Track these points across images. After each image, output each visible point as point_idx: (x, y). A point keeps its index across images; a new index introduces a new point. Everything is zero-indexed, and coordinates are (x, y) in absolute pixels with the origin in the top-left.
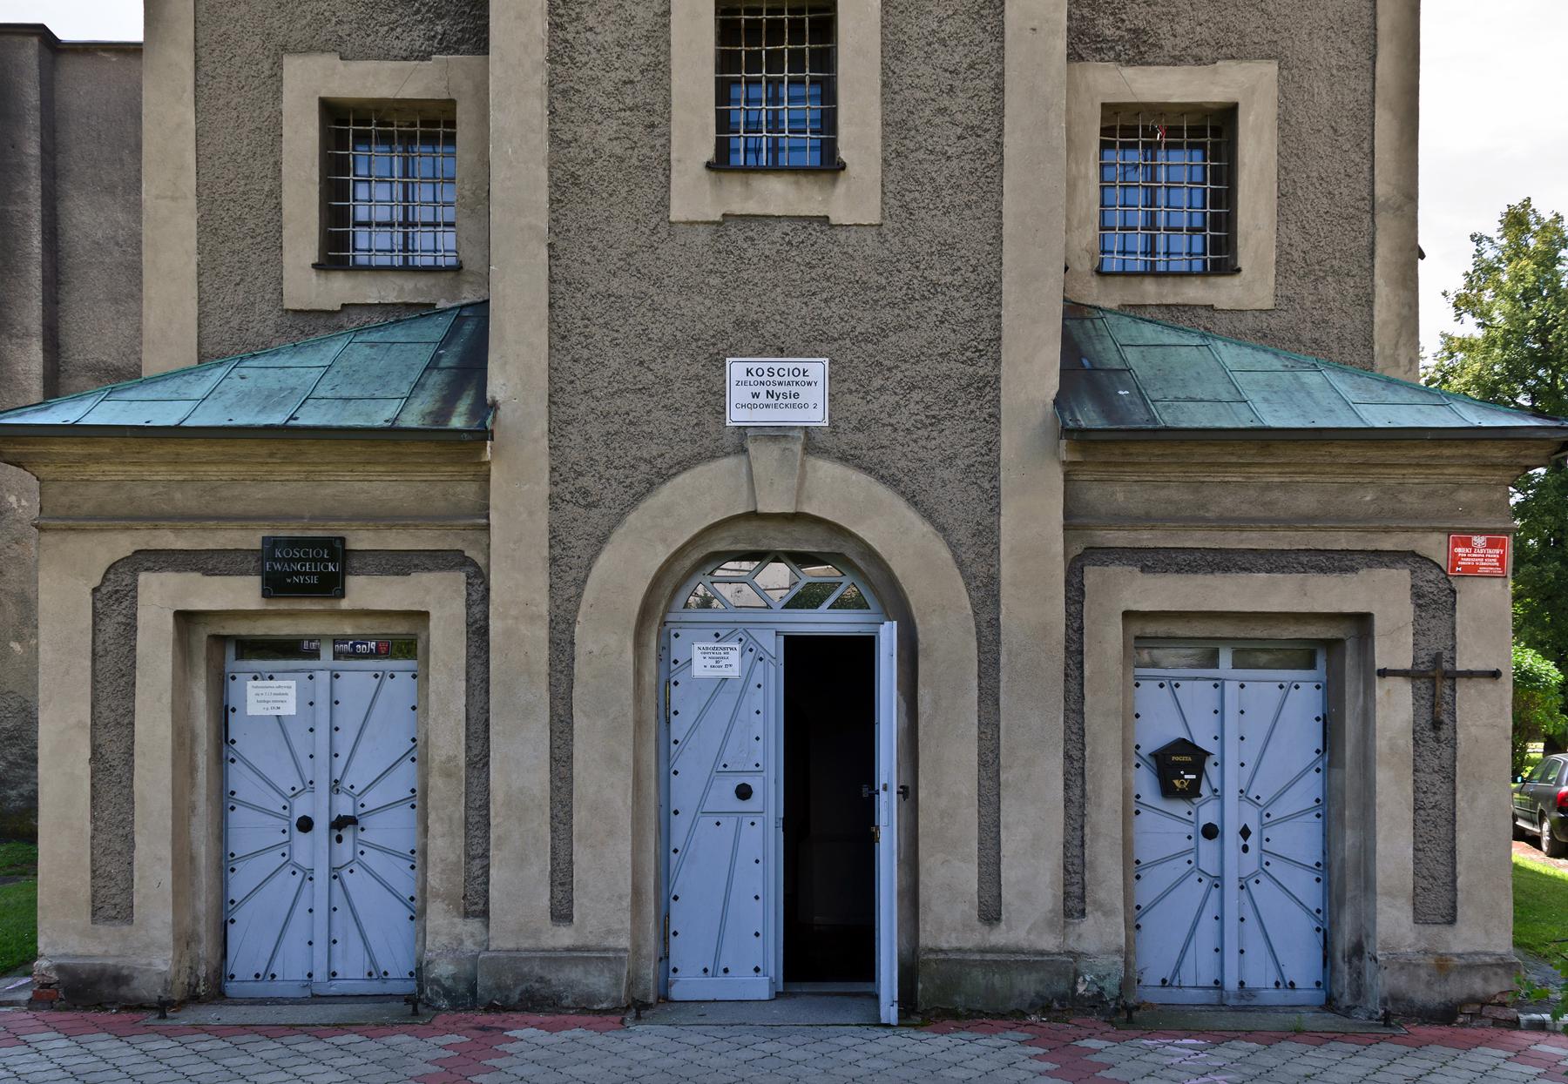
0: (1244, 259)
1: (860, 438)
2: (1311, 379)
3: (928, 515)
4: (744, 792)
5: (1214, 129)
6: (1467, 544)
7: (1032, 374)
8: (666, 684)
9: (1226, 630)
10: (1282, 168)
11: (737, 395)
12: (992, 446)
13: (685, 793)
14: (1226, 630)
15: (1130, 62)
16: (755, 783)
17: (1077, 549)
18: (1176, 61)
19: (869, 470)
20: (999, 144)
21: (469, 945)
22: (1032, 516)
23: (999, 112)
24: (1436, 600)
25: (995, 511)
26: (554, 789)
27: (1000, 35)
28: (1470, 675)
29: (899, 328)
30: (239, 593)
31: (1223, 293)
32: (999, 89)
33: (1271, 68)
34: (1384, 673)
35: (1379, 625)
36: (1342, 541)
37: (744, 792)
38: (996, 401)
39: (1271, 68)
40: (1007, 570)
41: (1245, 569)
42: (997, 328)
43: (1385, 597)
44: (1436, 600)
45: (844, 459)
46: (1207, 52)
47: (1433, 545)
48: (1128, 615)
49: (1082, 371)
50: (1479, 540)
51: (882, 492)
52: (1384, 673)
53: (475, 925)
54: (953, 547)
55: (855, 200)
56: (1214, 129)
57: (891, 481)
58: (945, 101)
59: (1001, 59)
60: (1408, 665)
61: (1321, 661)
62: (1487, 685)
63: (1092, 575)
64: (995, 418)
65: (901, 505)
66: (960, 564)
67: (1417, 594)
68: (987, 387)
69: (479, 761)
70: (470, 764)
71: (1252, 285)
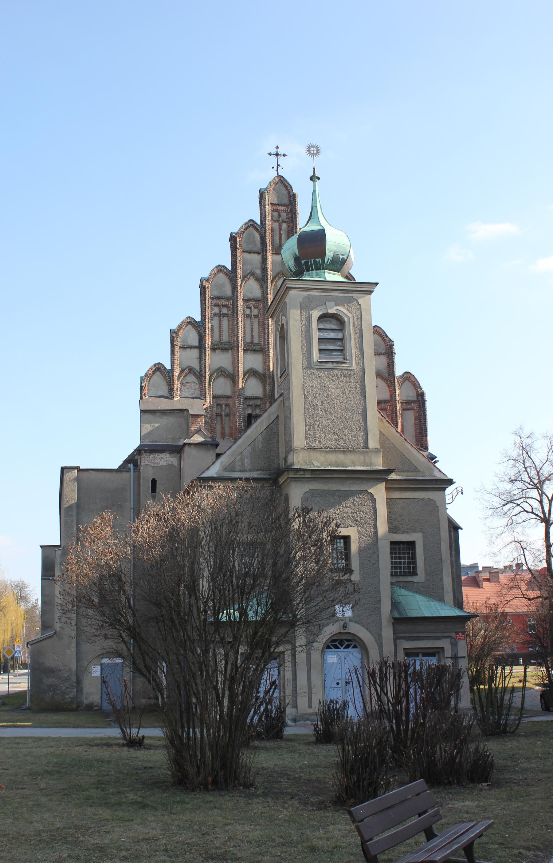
0: (418, 572)
1: (358, 618)
2: (432, 603)
3: (370, 632)
4: (338, 684)
5: (412, 544)
6: (458, 634)
7: (386, 607)
8: (324, 663)
9: (420, 651)
10: (425, 554)
12: (380, 619)
13: (328, 684)
14: (420, 651)
15: (395, 533)
16: (340, 682)
17: (395, 637)
18: (403, 532)
19: (359, 624)
20: (379, 567)
21: (293, 713)
22: (388, 633)
23: (378, 561)
24: (454, 645)
25: (381, 631)
26: (308, 684)
27: (378, 547)
28: (461, 657)
29: (363, 599)
31: (415, 579)
32: (378, 557)
33: (421, 534)
34: (447, 658)
35: (445, 649)
36: (439, 634)
37: (338, 684)
38: (380, 611)
39: (421, 534)
40: (384, 641)
41: (148, 749)
42: (380, 598)
43: (445, 644)
44: (454, 645)
45: (355, 622)
46: (409, 531)
47: (453, 635)
48: (404, 649)
49: (395, 605)
50: (460, 634)
51: (362, 628)
52: (447, 658)
53: (295, 709)
54: (374, 637)
56: (412, 544)
57: (363, 626)
58: (369, 559)
59: (378, 552)
60: (450, 656)
61: (437, 655)
62: (463, 659)
63: (398, 642)
64: (380, 614)
65: (365, 630)
66: (376, 641)
67: (451, 643)
68: (379, 609)
69: (295, 679)
70: (293, 680)
71: (420, 577)
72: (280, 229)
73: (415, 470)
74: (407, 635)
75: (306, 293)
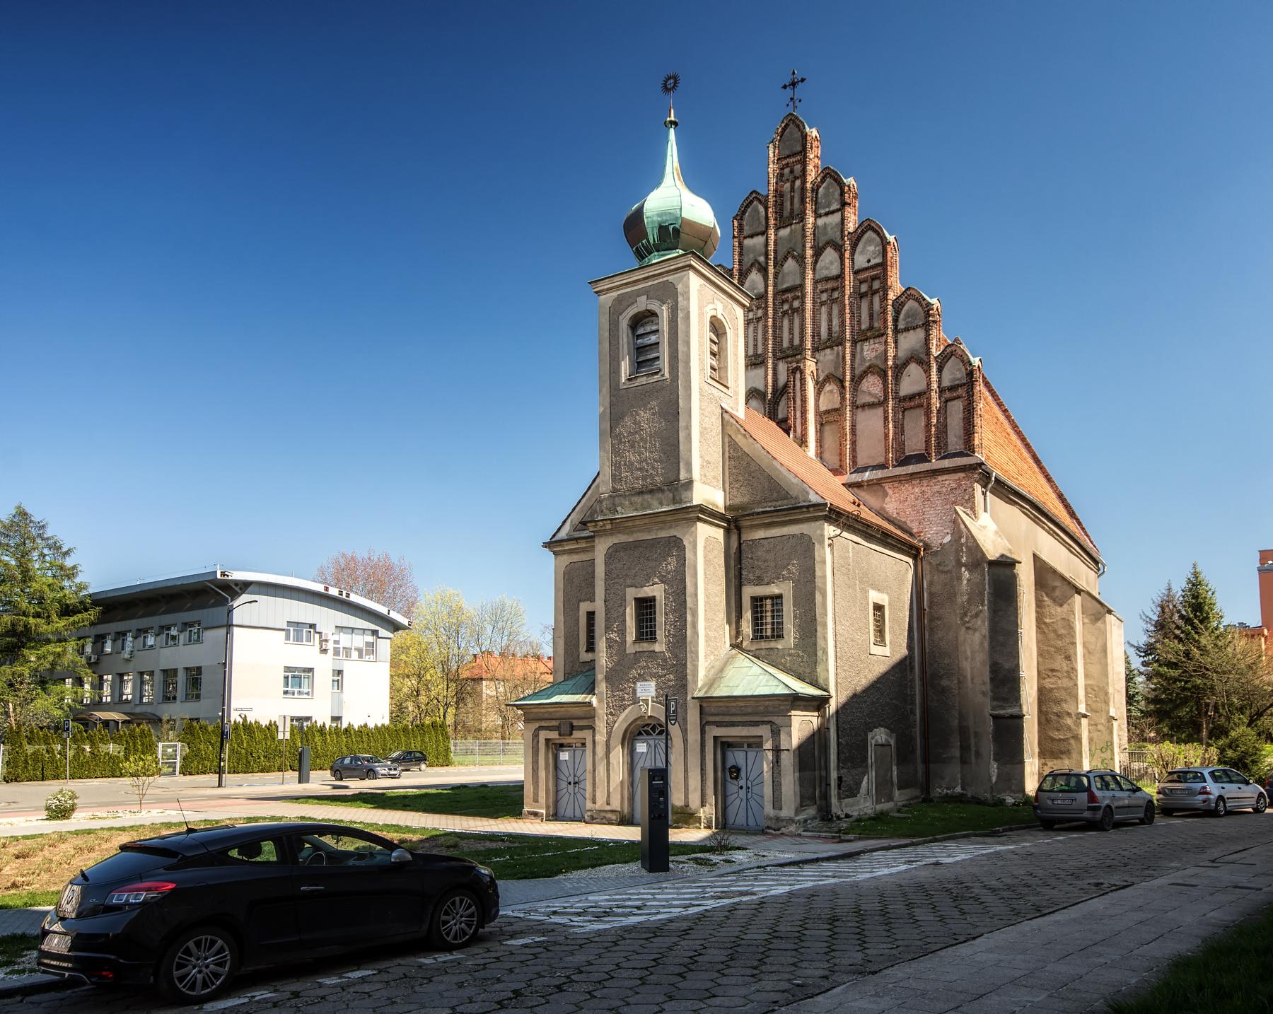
11: (638, 690)
30: (553, 735)
31: (780, 645)
47: (774, 719)
55: (659, 647)
72: (792, 189)
73: (787, 496)
74: (717, 719)
75: (615, 294)
